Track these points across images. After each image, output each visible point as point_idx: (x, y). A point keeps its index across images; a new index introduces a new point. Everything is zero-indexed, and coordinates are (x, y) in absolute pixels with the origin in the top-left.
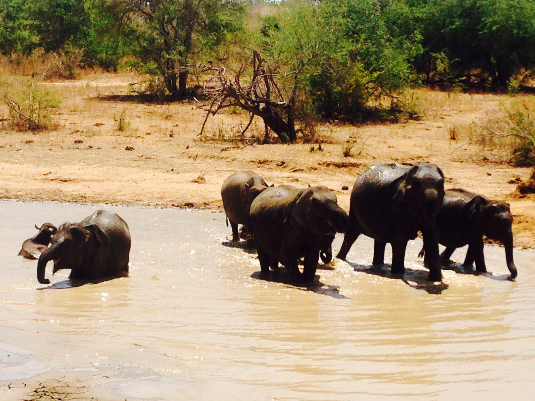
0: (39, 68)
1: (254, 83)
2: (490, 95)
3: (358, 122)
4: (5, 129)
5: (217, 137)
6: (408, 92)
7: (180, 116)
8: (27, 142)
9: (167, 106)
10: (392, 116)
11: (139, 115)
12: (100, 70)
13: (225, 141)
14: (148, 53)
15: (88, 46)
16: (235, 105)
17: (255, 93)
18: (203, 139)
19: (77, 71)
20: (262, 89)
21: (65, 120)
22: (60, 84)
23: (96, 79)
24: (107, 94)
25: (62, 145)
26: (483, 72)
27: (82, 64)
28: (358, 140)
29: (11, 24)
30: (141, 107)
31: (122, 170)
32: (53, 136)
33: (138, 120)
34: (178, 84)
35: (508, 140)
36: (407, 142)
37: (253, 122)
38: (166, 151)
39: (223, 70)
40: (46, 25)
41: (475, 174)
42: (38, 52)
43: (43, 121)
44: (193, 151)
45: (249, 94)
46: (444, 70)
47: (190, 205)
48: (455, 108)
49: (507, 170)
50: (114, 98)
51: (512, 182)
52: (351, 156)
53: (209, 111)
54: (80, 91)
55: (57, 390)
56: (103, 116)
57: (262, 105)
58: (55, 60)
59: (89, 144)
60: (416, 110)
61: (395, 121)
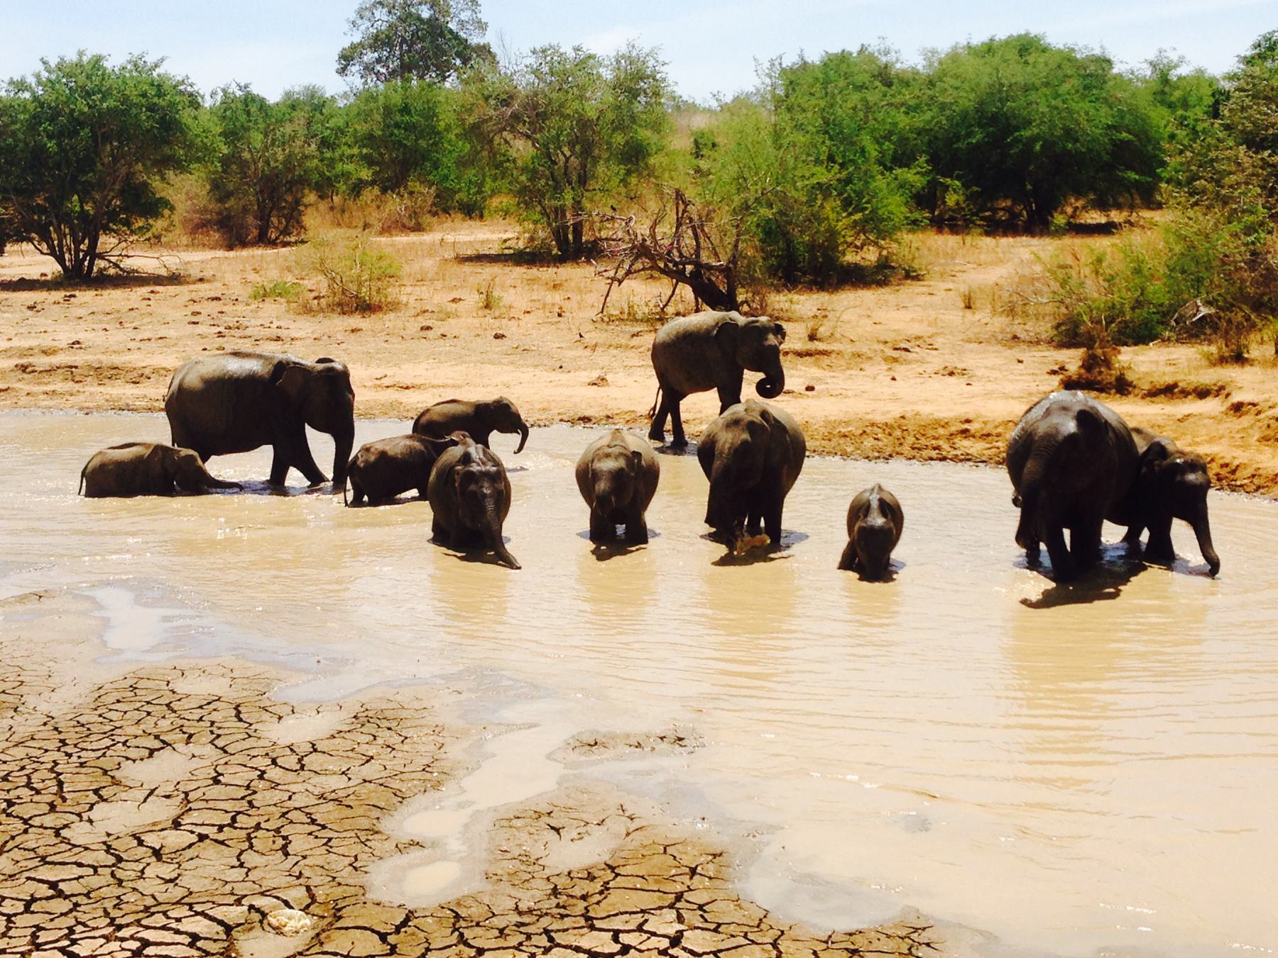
0: (374, 217)
1: (678, 236)
2: (1024, 238)
3: (830, 285)
4: (322, 310)
5: (625, 316)
6: (906, 237)
7: (573, 284)
8: (353, 331)
9: (555, 270)
10: (879, 276)
11: (515, 286)
12: (460, 216)
13: (637, 320)
14: (528, 197)
15: (441, 181)
16: (651, 268)
17: (680, 252)
18: (606, 319)
19: (427, 219)
20: (688, 241)
21: (406, 294)
22: (402, 239)
23: (454, 230)
24: (469, 253)
25: (402, 333)
26: (1014, 204)
27: (434, 209)
28: (830, 315)
29: (328, 155)
30: (520, 271)
31: (489, 369)
32: (388, 320)
33: (512, 291)
34: (570, 237)
35: (1049, 309)
36: (902, 314)
37: (677, 291)
38: (553, 339)
39: (631, 219)
40: (381, 155)
41: (999, 361)
42: (369, 194)
43: (376, 299)
44: (590, 338)
45: (669, 253)
46: (957, 204)
47: (586, 419)
48: (971, 260)
49: (1046, 354)
50: (480, 258)
51: (1054, 372)
52: (820, 340)
53: (613, 279)
54: (431, 250)
55: (387, 714)
56: (462, 287)
57: (689, 268)
58: (395, 205)
59: (442, 331)
60: (916, 266)
61: (883, 283)
